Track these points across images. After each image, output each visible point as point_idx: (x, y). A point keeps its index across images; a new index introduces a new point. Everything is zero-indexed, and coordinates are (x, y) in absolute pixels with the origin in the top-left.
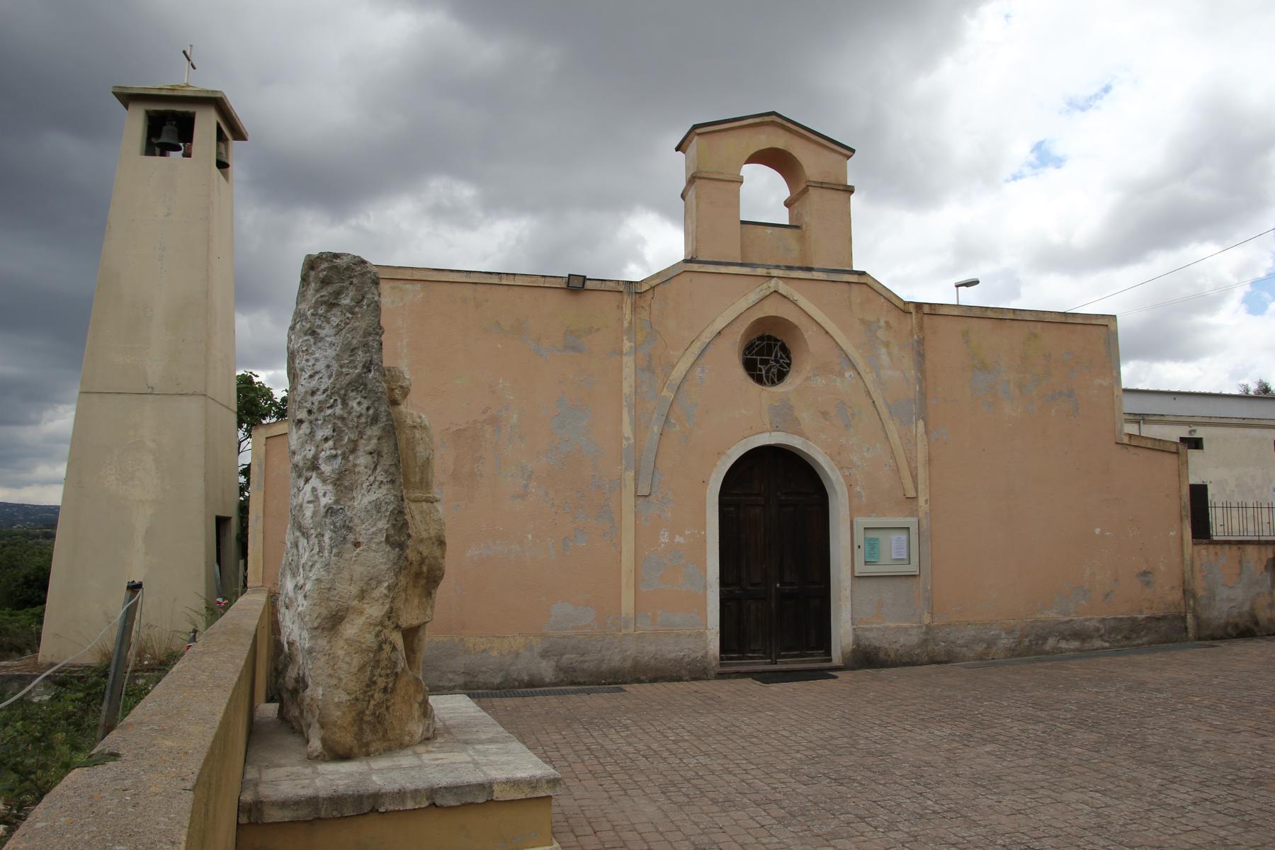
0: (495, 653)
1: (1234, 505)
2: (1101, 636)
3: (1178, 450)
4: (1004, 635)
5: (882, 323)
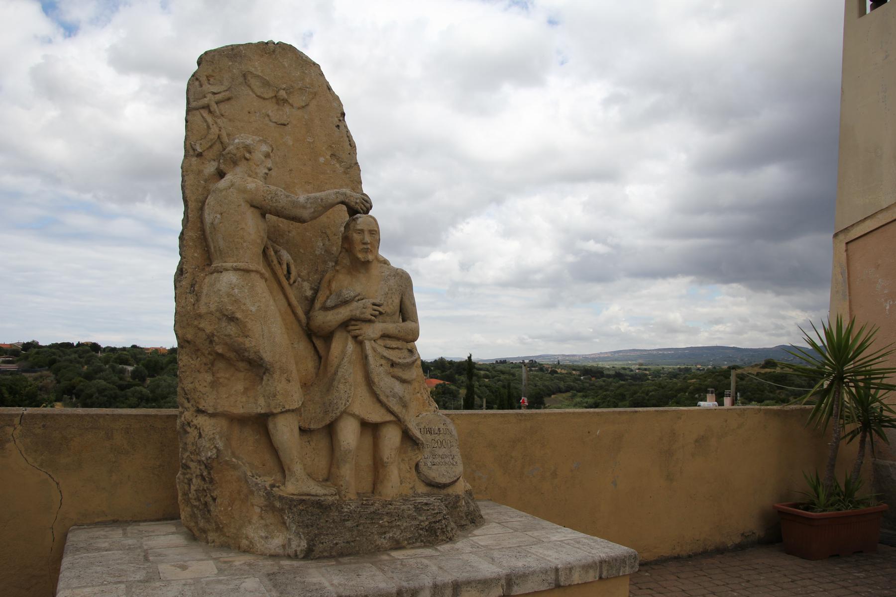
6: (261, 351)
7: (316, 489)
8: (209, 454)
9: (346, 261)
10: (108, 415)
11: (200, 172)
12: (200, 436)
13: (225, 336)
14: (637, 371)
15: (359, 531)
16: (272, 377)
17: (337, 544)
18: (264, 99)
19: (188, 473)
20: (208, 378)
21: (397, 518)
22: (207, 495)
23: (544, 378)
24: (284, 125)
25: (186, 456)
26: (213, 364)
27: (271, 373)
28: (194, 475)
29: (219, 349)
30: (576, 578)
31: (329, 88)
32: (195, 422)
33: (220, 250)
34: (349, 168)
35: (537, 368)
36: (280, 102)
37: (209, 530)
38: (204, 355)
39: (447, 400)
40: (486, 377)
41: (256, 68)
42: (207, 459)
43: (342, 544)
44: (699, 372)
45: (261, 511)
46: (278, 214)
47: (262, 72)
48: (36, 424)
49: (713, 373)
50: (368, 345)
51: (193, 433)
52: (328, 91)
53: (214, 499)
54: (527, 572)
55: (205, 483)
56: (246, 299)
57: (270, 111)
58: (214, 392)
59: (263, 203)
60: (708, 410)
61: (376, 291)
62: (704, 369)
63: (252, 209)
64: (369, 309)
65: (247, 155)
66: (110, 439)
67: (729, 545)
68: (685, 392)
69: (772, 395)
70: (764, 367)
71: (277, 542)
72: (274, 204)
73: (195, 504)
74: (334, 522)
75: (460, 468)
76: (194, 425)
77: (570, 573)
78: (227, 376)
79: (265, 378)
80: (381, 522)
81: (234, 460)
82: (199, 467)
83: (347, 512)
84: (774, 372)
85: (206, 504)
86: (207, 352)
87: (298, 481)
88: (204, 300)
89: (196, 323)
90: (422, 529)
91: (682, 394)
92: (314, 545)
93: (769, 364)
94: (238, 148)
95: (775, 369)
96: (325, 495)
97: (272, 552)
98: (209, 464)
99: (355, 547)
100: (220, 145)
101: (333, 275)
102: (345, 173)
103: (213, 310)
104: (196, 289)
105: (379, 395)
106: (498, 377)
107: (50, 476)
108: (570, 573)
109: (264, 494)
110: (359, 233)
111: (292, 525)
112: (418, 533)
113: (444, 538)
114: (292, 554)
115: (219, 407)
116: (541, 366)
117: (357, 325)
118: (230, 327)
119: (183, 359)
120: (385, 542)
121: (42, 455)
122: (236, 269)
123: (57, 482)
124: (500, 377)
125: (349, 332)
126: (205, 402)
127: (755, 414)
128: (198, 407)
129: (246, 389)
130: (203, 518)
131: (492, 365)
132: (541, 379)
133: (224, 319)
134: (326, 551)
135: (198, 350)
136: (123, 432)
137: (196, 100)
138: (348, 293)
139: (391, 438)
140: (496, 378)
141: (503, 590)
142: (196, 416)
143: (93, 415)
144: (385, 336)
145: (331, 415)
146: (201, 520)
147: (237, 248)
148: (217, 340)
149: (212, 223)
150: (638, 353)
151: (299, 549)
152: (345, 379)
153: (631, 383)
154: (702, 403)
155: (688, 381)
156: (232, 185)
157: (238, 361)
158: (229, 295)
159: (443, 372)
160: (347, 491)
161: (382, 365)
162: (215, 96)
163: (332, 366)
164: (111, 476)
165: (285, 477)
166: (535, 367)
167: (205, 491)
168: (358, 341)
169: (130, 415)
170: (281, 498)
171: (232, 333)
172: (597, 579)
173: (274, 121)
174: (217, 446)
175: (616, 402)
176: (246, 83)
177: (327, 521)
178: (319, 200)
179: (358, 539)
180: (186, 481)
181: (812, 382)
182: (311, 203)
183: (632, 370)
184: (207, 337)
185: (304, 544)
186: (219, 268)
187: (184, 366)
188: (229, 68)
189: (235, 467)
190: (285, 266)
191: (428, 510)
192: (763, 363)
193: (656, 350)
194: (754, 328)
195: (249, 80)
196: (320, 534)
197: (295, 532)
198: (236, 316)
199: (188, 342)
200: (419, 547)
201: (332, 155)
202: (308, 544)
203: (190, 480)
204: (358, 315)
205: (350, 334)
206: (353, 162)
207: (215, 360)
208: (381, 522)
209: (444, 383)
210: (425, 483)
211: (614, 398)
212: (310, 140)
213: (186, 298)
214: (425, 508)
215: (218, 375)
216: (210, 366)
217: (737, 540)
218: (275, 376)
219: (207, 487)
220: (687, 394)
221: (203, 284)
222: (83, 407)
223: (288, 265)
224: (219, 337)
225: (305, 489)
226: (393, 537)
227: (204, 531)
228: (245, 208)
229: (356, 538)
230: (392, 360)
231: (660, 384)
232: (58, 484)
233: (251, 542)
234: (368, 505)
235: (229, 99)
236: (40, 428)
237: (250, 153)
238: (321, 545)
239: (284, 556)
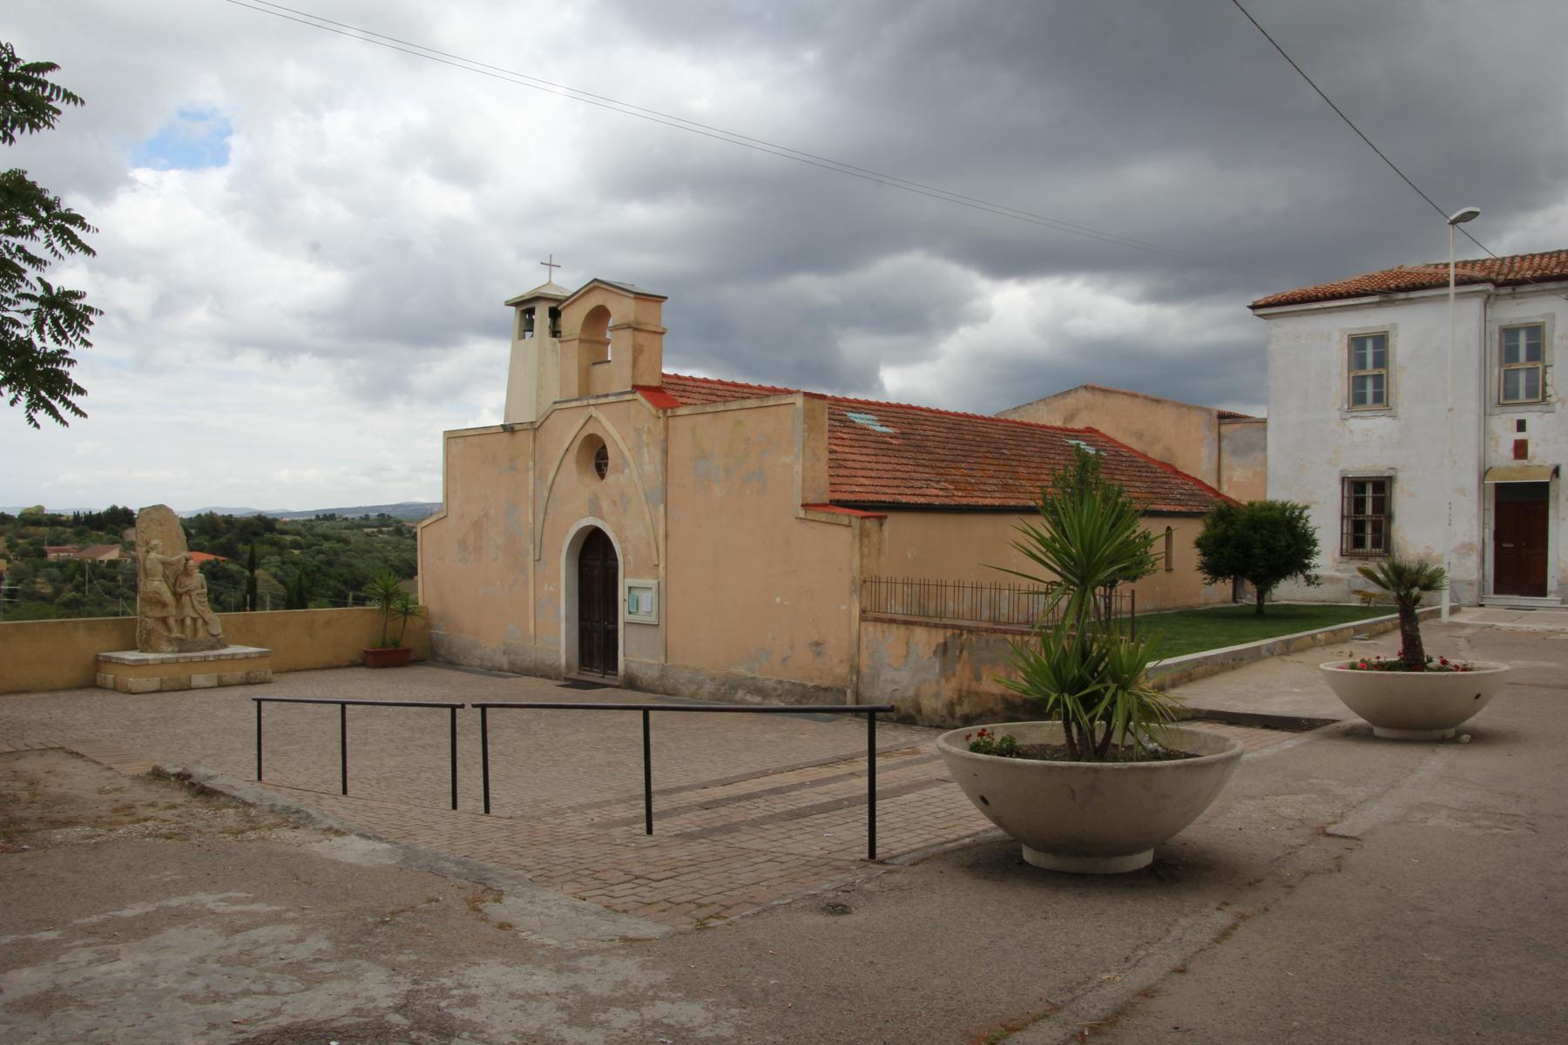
0: (488, 650)
1: (950, 583)
2: (779, 696)
3: (850, 523)
4: (708, 681)
5: (646, 429)
23: (401, 547)
30: (252, 656)
35: (391, 529)
36: (161, 525)
39: (221, 589)
40: (297, 545)
64: (546, 1007)
71: (170, 649)
106: (317, 547)
116: (399, 525)
124: (321, 545)
131: (308, 523)
132: (396, 548)
138: (187, 583)
139: (200, 622)
140: (314, 548)
144: (198, 594)
159: (214, 538)
166: (388, 526)
168: (190, 596)
209: (216, 560)
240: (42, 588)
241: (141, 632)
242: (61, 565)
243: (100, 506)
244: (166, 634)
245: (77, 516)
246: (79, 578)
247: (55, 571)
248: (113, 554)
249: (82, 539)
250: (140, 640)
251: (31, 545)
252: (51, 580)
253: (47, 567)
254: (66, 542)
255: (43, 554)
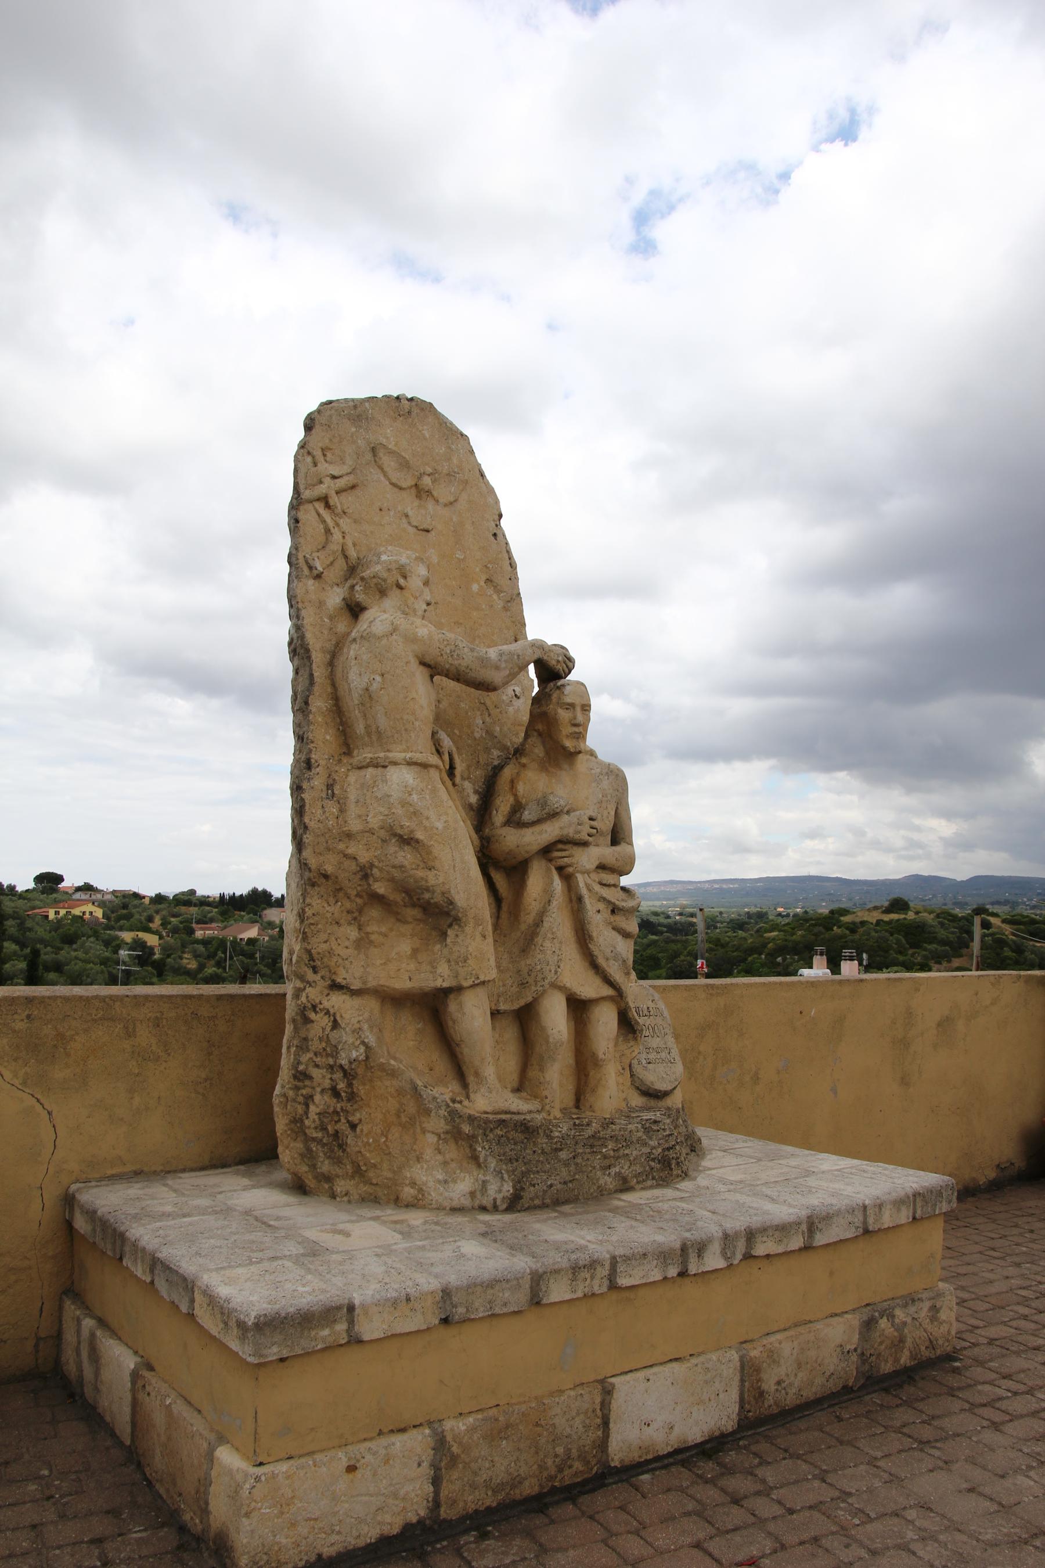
6: (452, 892)
7: (517, 1104)
8: (354, 1054)
9: (539, 751)
10: (127, 996)
11: (321, 604)
12: (335, 1025)
13: (394, 867)
14: (677, 918)
15: (577, 1164)
16: (463, 931)
17: (551, 1186)
18: (401, 489)
19: (305, 1087)
20: (353, 933)
21: (624, 1144)
22: (339, 1120)
24: (428, 531)
25: (307, 1058)
26: (360, 911)
27: (462, 925)
28: (319, 1089)
29: (381, 887)
30: (887, 1219)
31: (482, 475)
32: (326, 1004)
33: (379, 733)
34: (509, 601)
36: (421, 492)
37: (338, 1176)
38: (348, 898)
41: (387, 438)
42: (351, 1063)
43: (559, 1186)
44: (780, 919)
45: (438, 1141)
46: (458, 676)
47: (396, 445)
48: (16, 1013)
49: (806, 920)
50: (581, 880)
51: (321, 1021)
52: (481, 478)
53: (353, 1126)
54: (831, 1212)
55: (338, 1102)
56: (428, 809)
57: (409, 508)
58: (362, 956)
59: (440, 659)
60: (813, 984)
61: (587, 798)
62: (788, 915)
63: (422, 668)
65: (402, 581)
66: (130, 1036)
67: (981, 1183)
68: (761, 954)
69: (901, 958)
70: (888, 911)
71: (462, 1187)
72: (456, 662)
73: (315, 1135)
74: (543, 1152)
75: (679, 1068)
76: (324, 1009)
77: (880, 1212)
78: (384, 929)
79: (450, 932)
80: (604, 1150)
81: (392, 1062)
82: (329, 1076)
83: (558, 1137)
84: (905, 919)
85: (336, 1135)
86: (355, 893)
87: (490, 1092)
88: (353, 811)
89: (341, 846)
90: (653, 1160)
91: (755, 956)
92: (523, 1189)
93: (898, 905)
94: (389, 570)
95: (906, 914)
96: (530, 1112)
97: (455, 1204)
98: (352, 1069)
99: (573, 1190)
100: (343, 560)
101: (516, 771)
102: (506, 609)
103: (376, 826)
104: (336, 792)
105: (597, 957)
107: (38, 1101)
108: (880, 1212)
109: (446, 1113)
110: (567, 709)
111: (490, 1159)
112: (649, 1166)
113: (680, 1172)
114: (489, 1206)
115: (370, 979)
117: (565, 850)
118: (402, 854)
119: (313, 904)
120: (609, 1180)
121: (26, 1065)
122: (410, 763)
123: (50, 1110)
125: (550, 860)
126: (347, 972)
127: (1014, 982)
128: (333, 981)
129: (415, 951)
130: (329, 1157)
133: (393, 841)
134: (537, 1197)
135: (341, 889)
136: (150, 1024)
137: (310, 486)
141: (804, 1238)
142: (328, 995)
143: (106, 997)
145: (533, 988)
146: (322, 1162)
147: (406, 730)
148: (378, 873)
149: (367, 689)
150: (679, 887)
151: (499, 1197)
152: (553, 933)
153: (668, 938)
154: (805, 972)
155: (765, 935)
156: (395, 630)
157: (405, 906)
158: (404, 804)
160: (552, 1104)
161: (599, 911)
162: (336, 480)
163: (529, 914)
164: (132, 1098)
165: (465, 1085)
167: (338, 1113)
168: (567, 876)
169: (162, 996)
170: (471, 1119)
171: (406, 863)
172: (911, 1220)
173: (415, 524)
174: (366, 1040)
175: (645, 970)
176: (375, 461)
177: (534, 1152)
178: (516, 657)
179: (577, 1177)
180: (301, 1099)
181: (965, 935)
182: (505, 661)
183: (668, 917)
184: (358, 869)
185: (508, 1188)
186: (379, 760)
187: (314, 915)
188: (352, 436)
189: (393, 1074)
190: (446, 757)
191: (658, 1131)
192: (886, 904)
193: (708, 881)
194: (876, 845)
195: (380, 458)
196: (529, 1172)
197: (495, 1170)
198: (416, 837)
199: (326, 877)
200: (651, 1187)
201: (488, 581)
202: (514, 1187)
203: (310, 1098)
204: (571, 835)
205: (554, 863)
206: (515, 592)
207: (365, 904)
208: (604, 1150)
210: (640, 1090)
211: (641, 964)
212: (459, 555)
213: (323, 807)
214: (655, 1128)
215: (369, 929)
216: (356, 914)
217: (992, 1174)
218: (467, 929)
219: (342, 1109)
220: (763, 956)
221: (346, 785)
222: (26, 985)
223: (450, 755)
224: (381, 870)
225: (502, 1105)
226: (620, 1173)
227: (328, 1179)
228: (414, 664)
229: (575, 1174)
230: (614, 904)
231: (718, 940)
232: (50, 1113)
233: (420, 1190)
234: (582, 1125)
235: (353, 487)
236: (22, 1020)
237: (405, 577)
238: (532, 1188)
239: (473, 1208)
240: (189, 963)
241: (301, 1076)
242: (206, 942)
243: (242, 889)
244: (445, 1092)
245: (222, 897)
246: (220, 954)
247: (201, 948)
248: (252, 932)
249: (226, 919)
250: (297, 1123)
251: (181, 922)
252: (196, 956)
253: (193, 943)
254: (212, 920)
255: (192, 932)
